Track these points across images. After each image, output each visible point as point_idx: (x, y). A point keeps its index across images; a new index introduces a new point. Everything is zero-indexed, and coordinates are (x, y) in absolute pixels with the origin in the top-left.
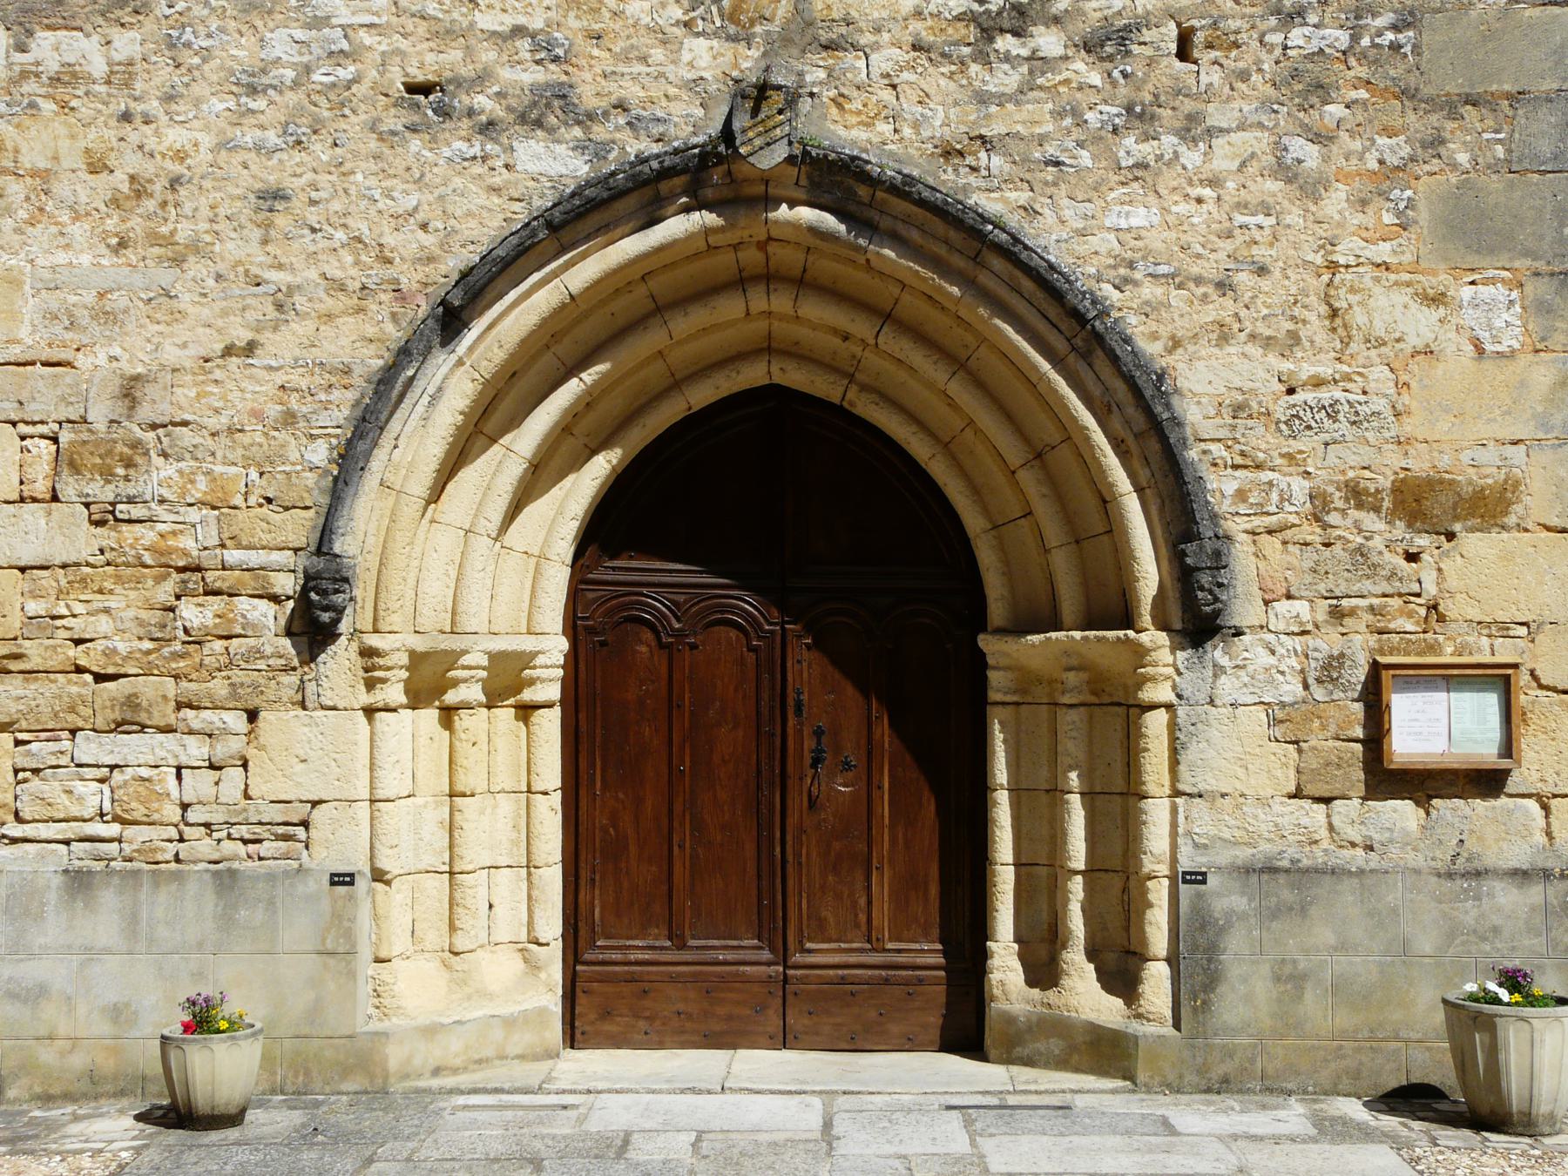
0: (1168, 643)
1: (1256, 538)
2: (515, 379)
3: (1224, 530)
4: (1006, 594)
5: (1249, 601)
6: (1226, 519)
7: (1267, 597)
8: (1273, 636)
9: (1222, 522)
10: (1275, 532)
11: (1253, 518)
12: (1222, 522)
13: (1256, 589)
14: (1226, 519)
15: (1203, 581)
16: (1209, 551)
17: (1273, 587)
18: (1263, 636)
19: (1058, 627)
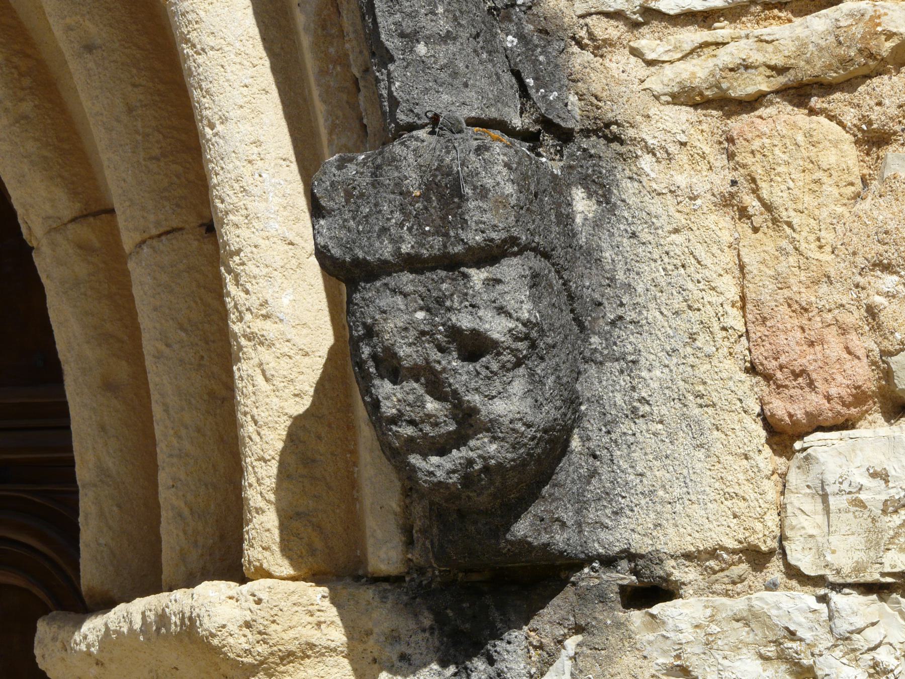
0: (337, 635)
1: (738, 124)
2: (805, 71)
3: (593, 100)
4: (110, 463)
5: (694, 426)
6: (599, 47)
7: (779, 408)
8: (807, 598)
9: (580, 58)
10: (826, 88)
11: (723, 30)
12: (580, 58)
13: (732, 369)
14: (599, 47)
15: (390, 327)
16: (413, 182)
17: (807, 359)
18: (764, 600)
19: (155, 588)
